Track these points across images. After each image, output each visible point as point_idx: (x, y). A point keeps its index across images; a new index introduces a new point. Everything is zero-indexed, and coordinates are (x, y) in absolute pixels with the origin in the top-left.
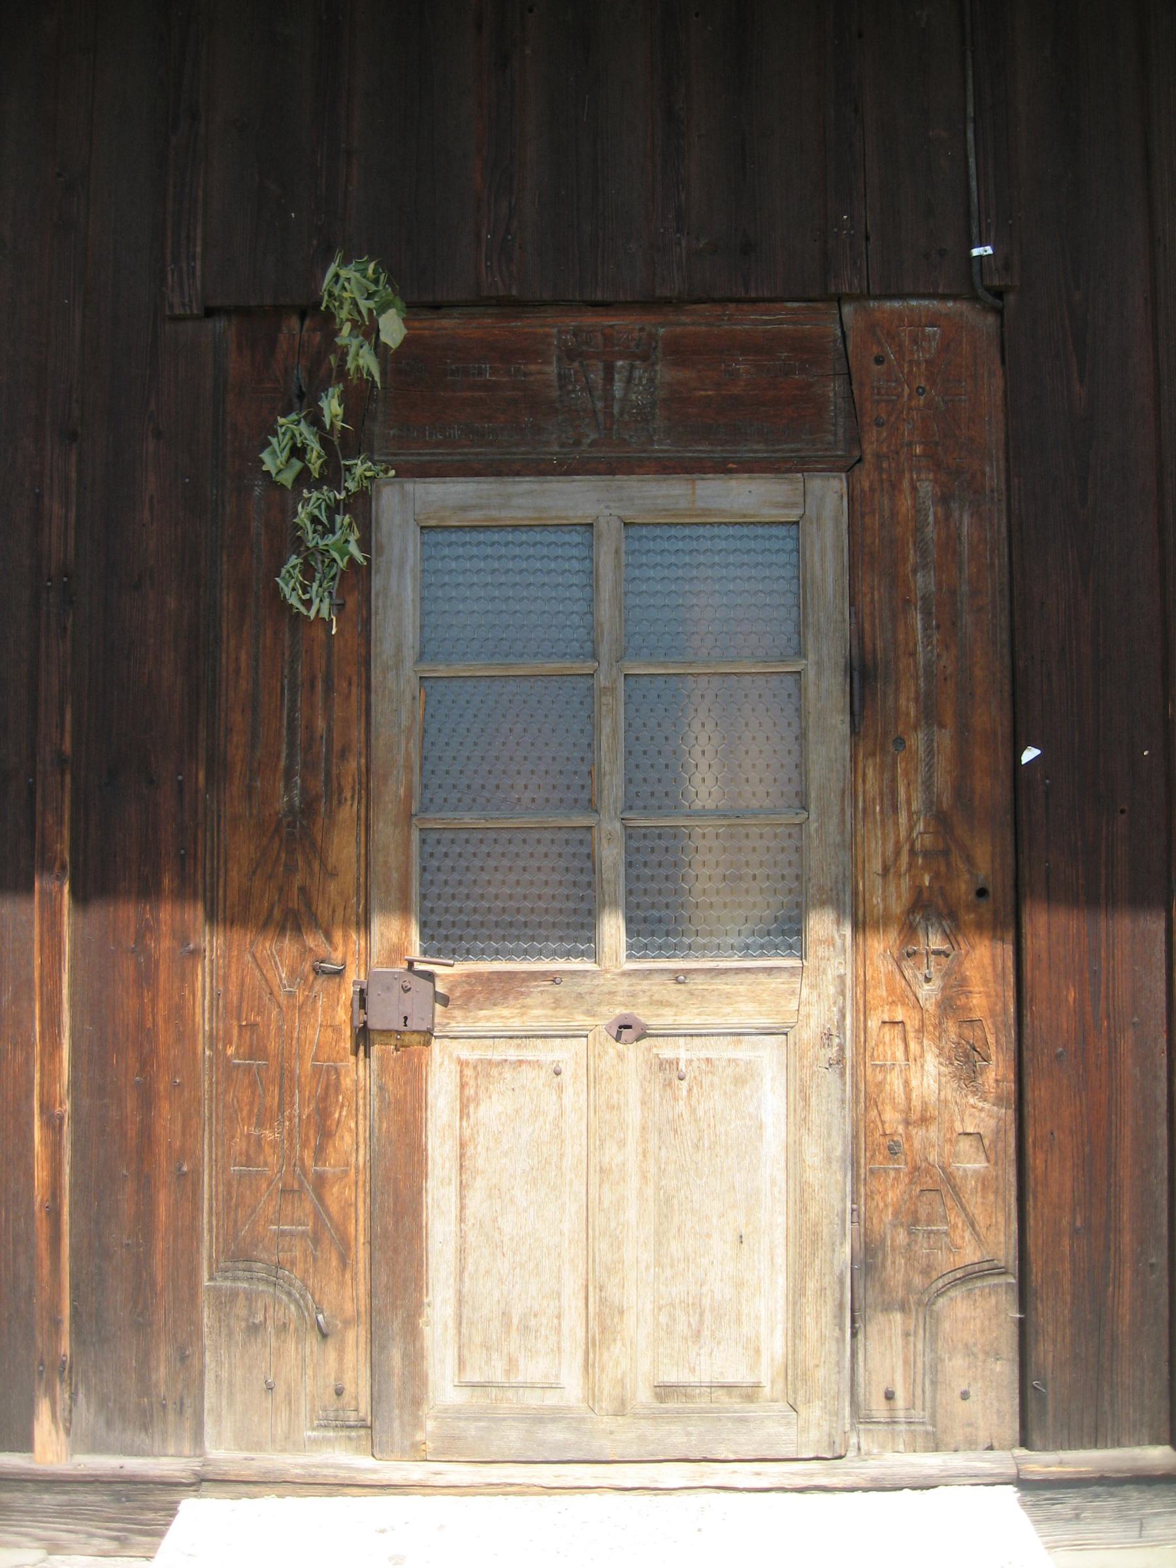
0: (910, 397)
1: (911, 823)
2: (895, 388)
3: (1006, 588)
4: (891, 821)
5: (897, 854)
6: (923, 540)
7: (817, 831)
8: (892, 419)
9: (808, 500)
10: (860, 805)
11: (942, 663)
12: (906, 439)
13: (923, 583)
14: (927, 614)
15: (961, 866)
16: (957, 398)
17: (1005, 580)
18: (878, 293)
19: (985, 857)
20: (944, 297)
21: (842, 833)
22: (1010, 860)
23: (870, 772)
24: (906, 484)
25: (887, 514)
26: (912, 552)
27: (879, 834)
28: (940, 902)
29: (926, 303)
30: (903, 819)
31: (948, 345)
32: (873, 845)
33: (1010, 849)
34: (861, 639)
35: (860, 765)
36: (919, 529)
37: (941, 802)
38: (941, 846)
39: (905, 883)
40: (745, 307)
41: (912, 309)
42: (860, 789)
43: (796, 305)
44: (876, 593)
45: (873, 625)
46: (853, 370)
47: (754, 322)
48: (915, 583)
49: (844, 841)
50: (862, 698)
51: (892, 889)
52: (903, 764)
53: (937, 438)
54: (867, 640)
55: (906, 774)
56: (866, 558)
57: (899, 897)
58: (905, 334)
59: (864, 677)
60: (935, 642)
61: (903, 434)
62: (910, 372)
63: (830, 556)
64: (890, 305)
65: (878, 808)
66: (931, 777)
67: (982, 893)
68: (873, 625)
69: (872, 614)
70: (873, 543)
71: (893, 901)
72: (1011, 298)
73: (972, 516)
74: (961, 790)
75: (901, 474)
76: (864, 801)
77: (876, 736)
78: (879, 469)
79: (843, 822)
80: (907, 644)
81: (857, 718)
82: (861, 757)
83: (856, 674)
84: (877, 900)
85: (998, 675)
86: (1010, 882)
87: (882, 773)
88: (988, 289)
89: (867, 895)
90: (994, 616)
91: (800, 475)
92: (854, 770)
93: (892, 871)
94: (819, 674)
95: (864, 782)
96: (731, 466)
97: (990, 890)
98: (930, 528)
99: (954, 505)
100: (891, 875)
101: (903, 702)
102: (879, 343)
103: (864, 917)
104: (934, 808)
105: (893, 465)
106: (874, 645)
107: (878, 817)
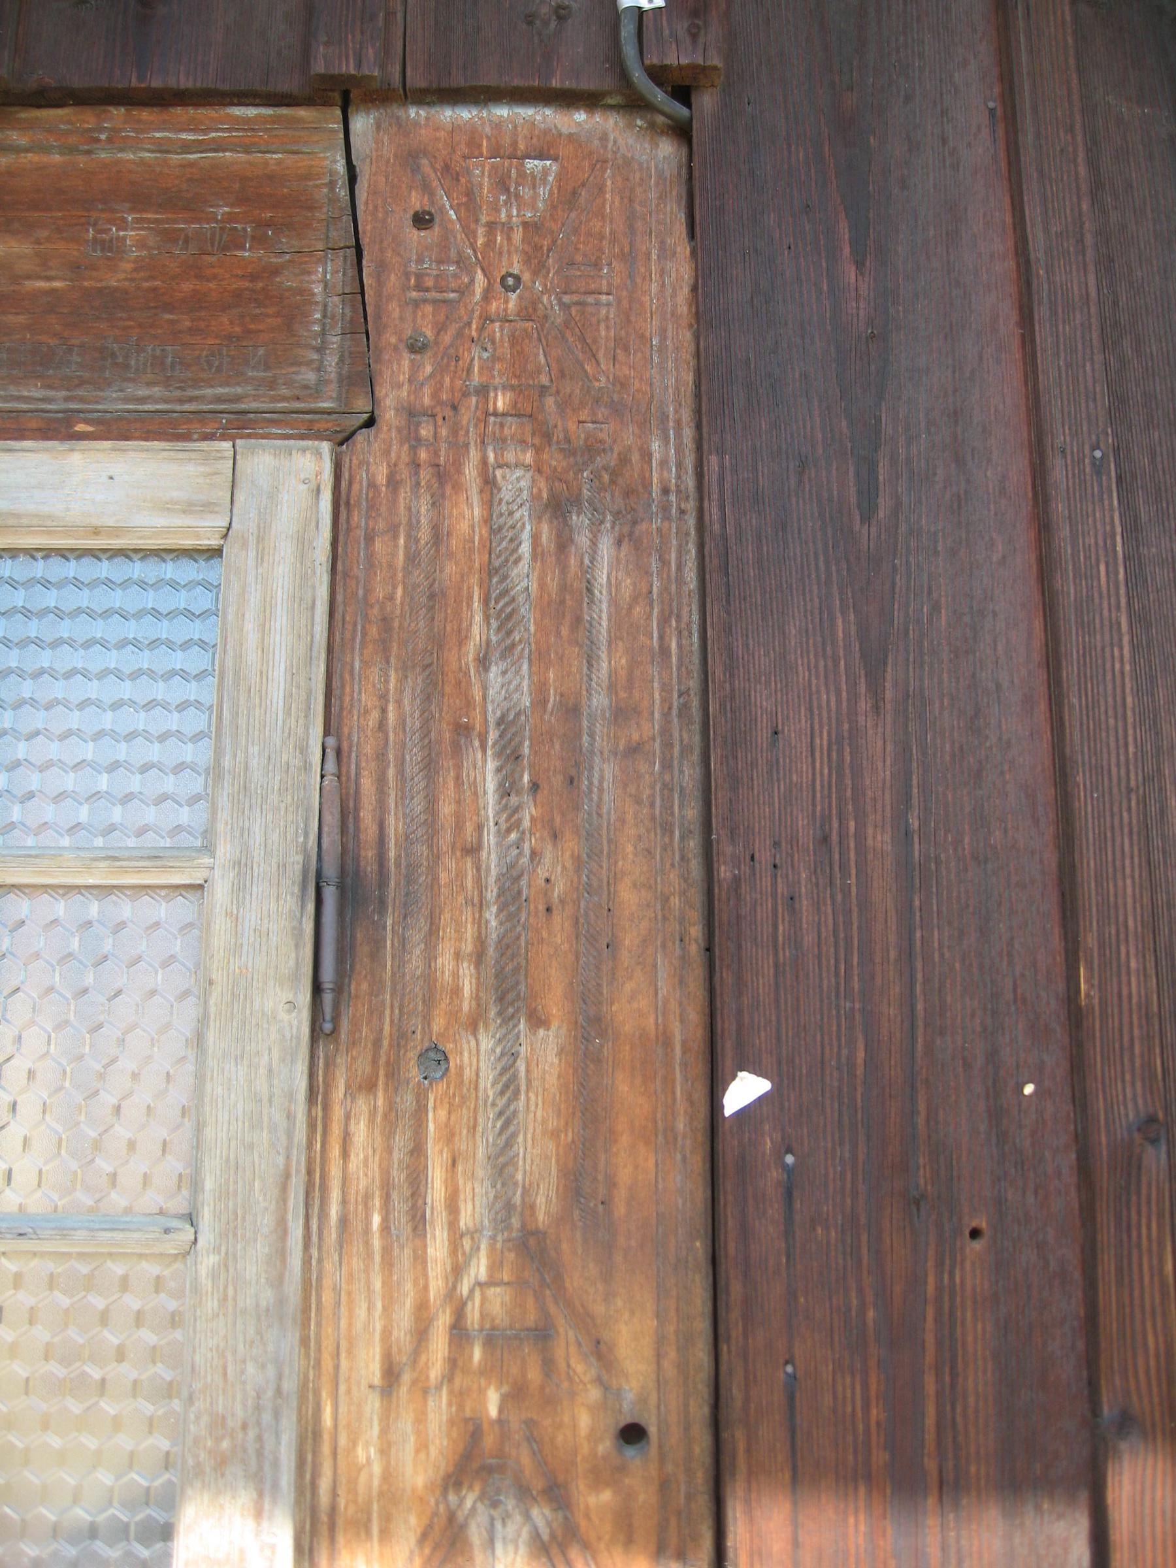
0: (487, 296)
1: (460, 1261)
2: (455, 276)
3: (695, 703)
4: (407, 1252)
5: (421, 1334)
6: (506, 592)
7: (214, 1275)
8: (447, 338)
9: (240, 497)
10: (334, 1211)
11: (542, 873)
12: (476, 379)
13: (503, 688)
14: (510, 757)
15: (580, 1368)
16: (590, 299)
17: (694, 684)
18: (423, 84)
19: (640, 1346)
20: (567, 99)
21: (278, 1282)
22: (701, 1354)
23: (360, 1131)
24: (470, 472)
25: (424, 535)
26: (478, 618)
27: (378, 1285)
28: (526, 1459)
29: (527, 112)
30: (437, 1248)
31: (574, 193)
32: (361, 1312)
33: (702, 1326)
34: (348, 814)
35: (338, 1113)
36: (495, 571)
37: (532, 1207)
38: (531, 1318)
39: (439, 1409)
40: (145, 114)
41: (498, 125)
42: (335, 1171)
43: (251, 112)
44: (391, 707)
45: (381, 781)
46: (365, 241)
47: (162, 147)
48: (485, 688)
49: (281, 1301)
50: (344, 952)
51: (405, 1424)
52: (443, 1113)
53: (544, 380)
54: (367, 816)
55: (449, 1136)
56: (373, 631)
57: (422, 1446)
58: (481, 174)
59: (350, 901)
60: (526, 824)
61: (469, 370)
62: (490, 243)
63: (281, 621)
64: (448, 114)
65: (376, 1220)
66: (509, 1144)
67: (632, 1434)
68: (381, 781)
69: (381, 757)
70: (391, 598)
71: (406, 1453)
72: (706, 101)
73: (619, 542)
74: (582, 1181)
75: (460, 449)
76: (344, 1202)
77: (377, 1043)
78: (415, 442)
79: (282, 1253)
80: (459, 826)
81: (328, 998)
82: (339, 1092)
83: (330, 894)
84: (367, 1453)
85: (675, 901)
86: (700, 1411)
87: (389, 1136)
88: (657, 75)
89: (343, 1441)
90: (667, 765)
91: (227, 445)
92: (319, 1126)
93: (406, 1378)
94: (239, 890)
95: (345, 1154)
96: (81, 427)
97: (652, 1430)
98: (524, 566)
99: (580, 521)
100: (404, 1389)
101: (445, 961)
102: (427, 188)
103: (334, 1494)
104: (515, 1222)
105: (444, 432)
106: (382, 827)
107: (376, 1243)
